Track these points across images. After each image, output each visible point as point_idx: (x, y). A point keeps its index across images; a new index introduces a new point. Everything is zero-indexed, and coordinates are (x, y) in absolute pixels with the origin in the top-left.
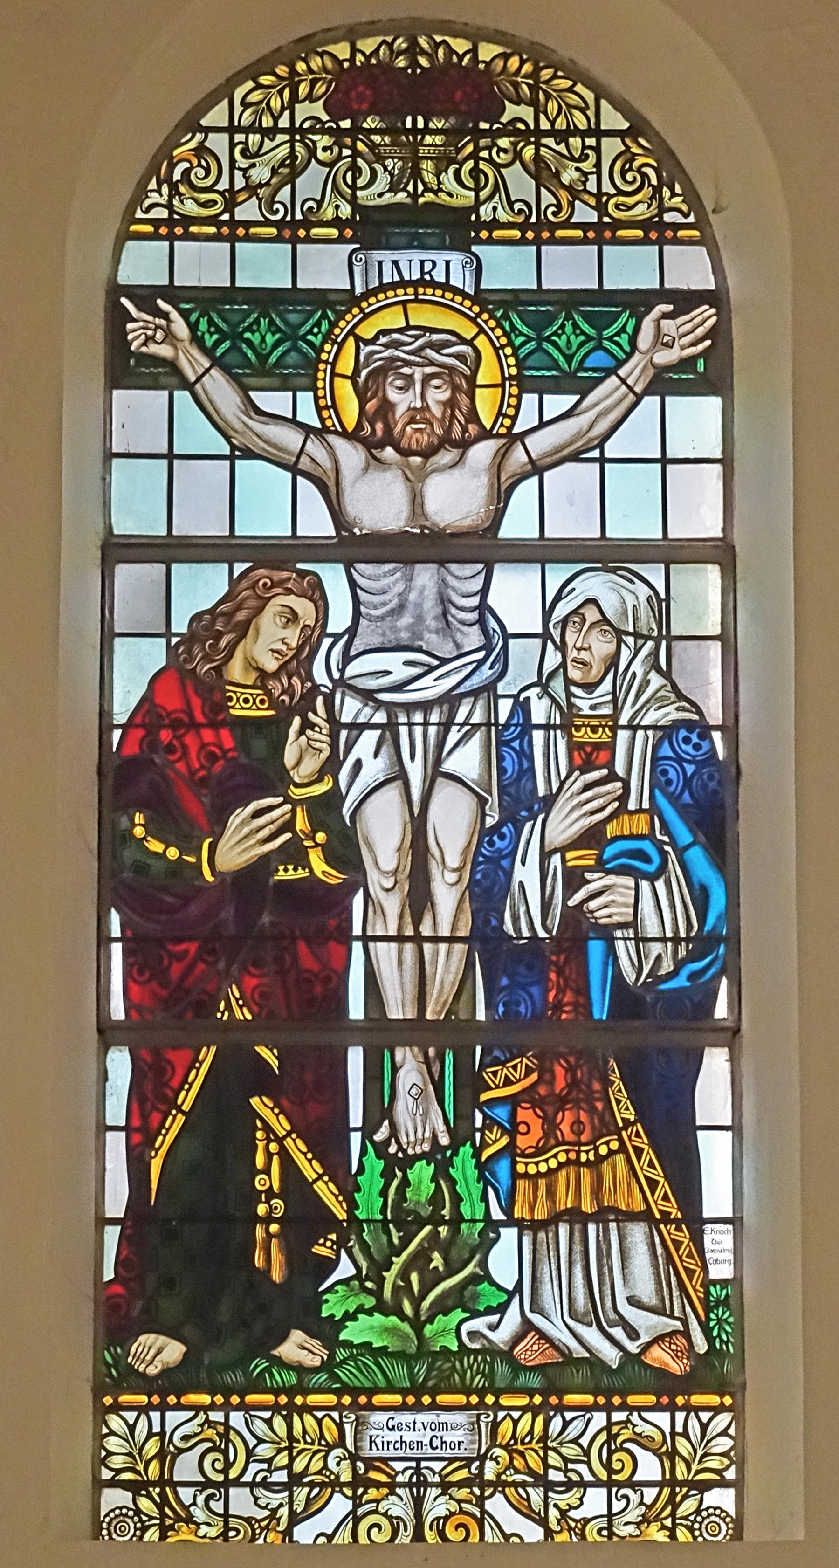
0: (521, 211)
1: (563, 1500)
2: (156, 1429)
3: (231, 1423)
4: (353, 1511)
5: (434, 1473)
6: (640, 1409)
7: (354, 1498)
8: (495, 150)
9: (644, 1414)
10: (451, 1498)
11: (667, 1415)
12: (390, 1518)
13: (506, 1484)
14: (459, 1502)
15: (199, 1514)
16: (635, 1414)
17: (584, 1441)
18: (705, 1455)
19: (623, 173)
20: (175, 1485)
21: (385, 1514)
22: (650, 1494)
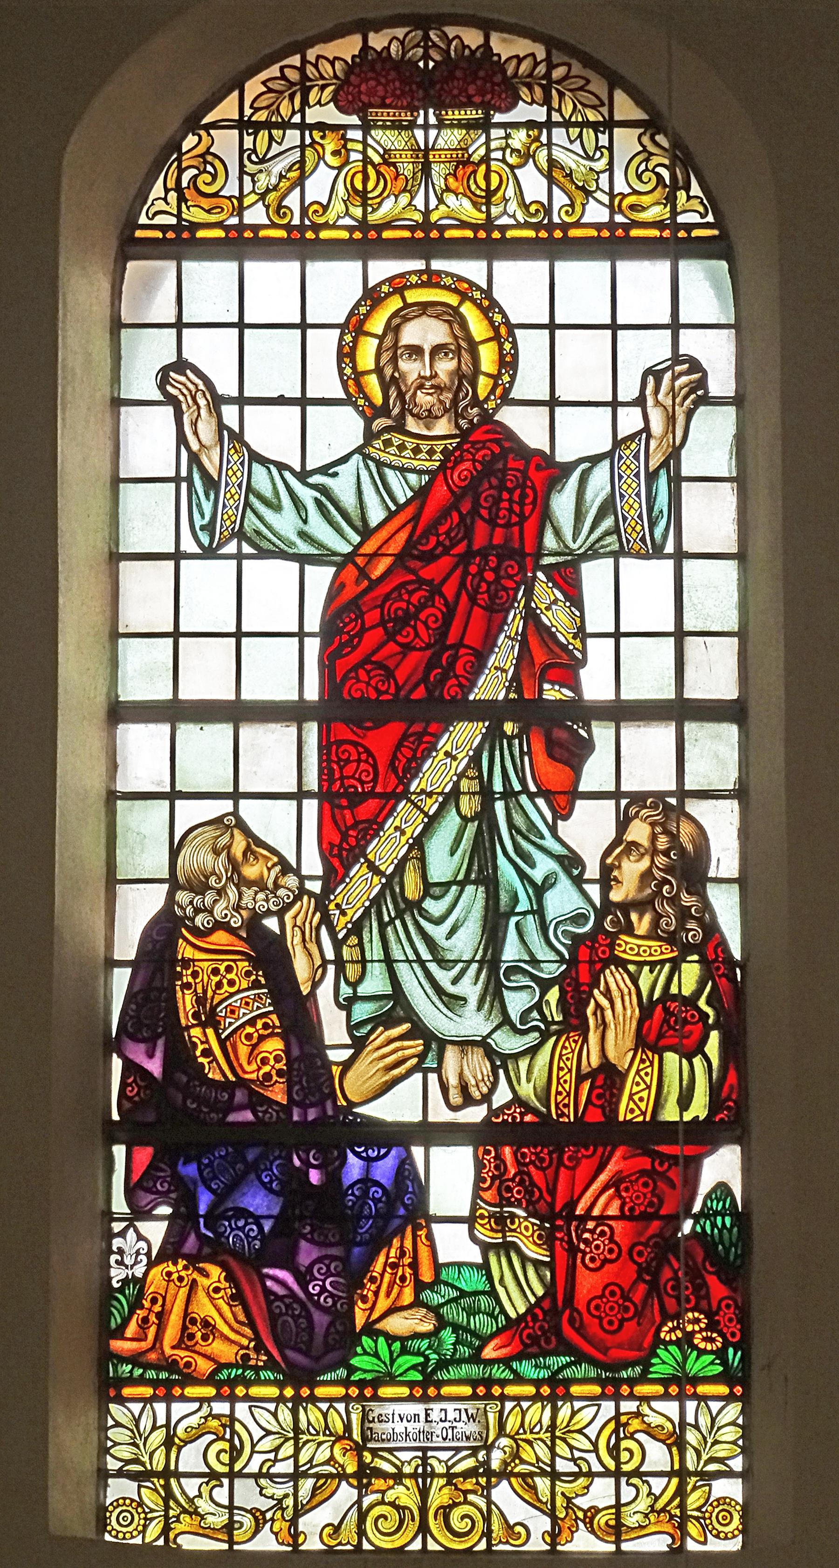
0: (537, 211)
2: (162, 1420)
4: (359, 1502)
5: (440, 1462)
8: (508, 151)
9: (653, 1404)
10: (457, 1489)
11: (675, 1405)
13: (512, 1474)
15: (204, 1505)
17: (592, 1432)
18: (716, 1442)
19: (639, 177)
20: (178, 1475)
21: (392, 1504)
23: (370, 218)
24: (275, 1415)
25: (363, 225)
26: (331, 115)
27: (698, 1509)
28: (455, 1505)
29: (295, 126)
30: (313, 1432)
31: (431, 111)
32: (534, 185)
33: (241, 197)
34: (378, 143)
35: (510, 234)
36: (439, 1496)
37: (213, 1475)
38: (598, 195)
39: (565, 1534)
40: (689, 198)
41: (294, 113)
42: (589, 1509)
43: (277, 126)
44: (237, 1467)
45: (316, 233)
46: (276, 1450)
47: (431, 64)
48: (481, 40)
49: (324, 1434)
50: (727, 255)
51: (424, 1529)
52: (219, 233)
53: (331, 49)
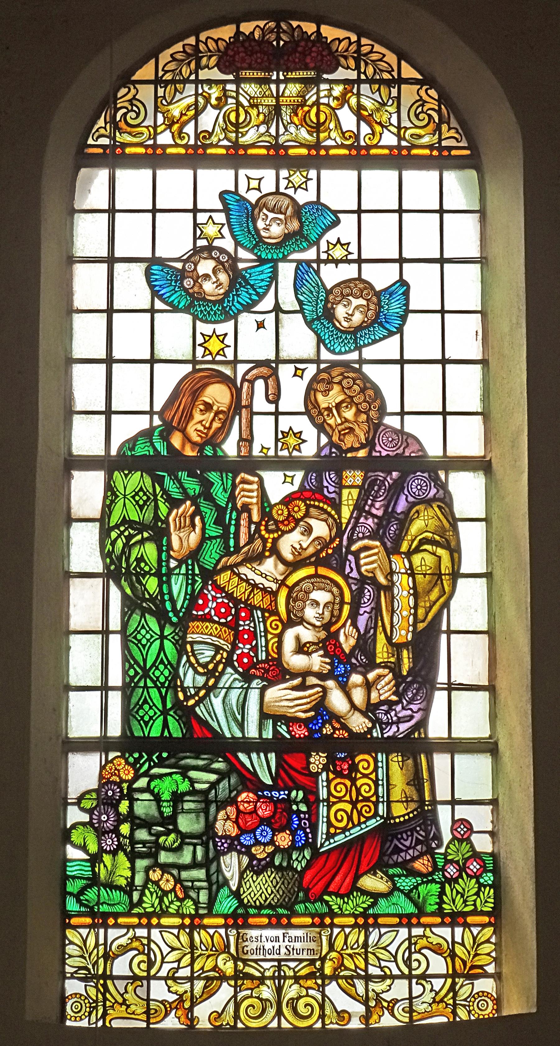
0: (350, 137)
1: (378, 987)
2: (101, 941)
3: (152, 938)
4: (235, 996)
6: (430, 926)
7: (235, 987)
9: (433, 929)
12: (261, 1000)
14: (307, 989)
16: (428, 929)
17: (392, 949)
18: (476, 955)
19: (417, 116)
21: (258, 998)
22: (437, 983)
23: (240, 140)
24: (178, 937)
25: (236, 145)
26: (216, 74)
27: (465, 1000)
28: (300, 997)
29: (192, 82)
30: (204, 948)
31: (281, 73)
32: (347, 119)
33: (155, 127)
34: (246, 92)
35: (332, 152)
36: (291, 991)
37: (135, 978)
38: (391, 128)
39: (375, 1017)
40: (450, 129)
41: (191, 74)
42: (391, 1001)
43: (179, 82)
44: (153, 972)
45: (205, 150)
46: (179, 961)
47: (282, 43)
48: (315, 29)
49: (211, 950)
50: (478, 168)
51: (279, 1013)
52: (141, 150)
53: (216, 33)
